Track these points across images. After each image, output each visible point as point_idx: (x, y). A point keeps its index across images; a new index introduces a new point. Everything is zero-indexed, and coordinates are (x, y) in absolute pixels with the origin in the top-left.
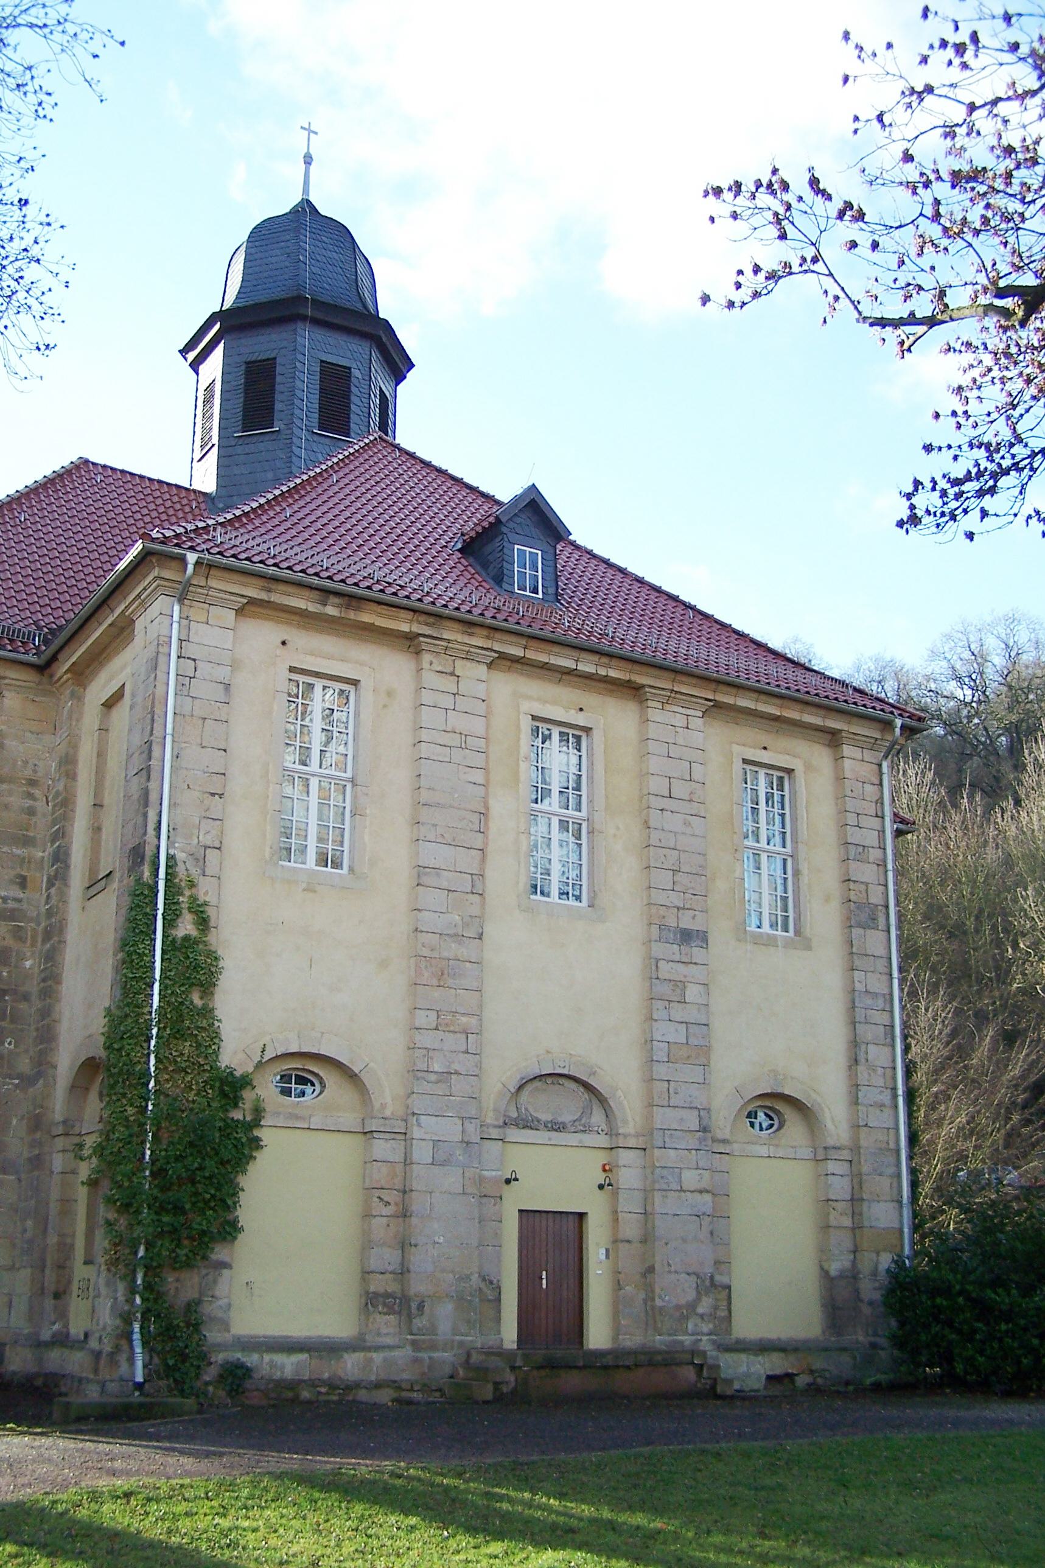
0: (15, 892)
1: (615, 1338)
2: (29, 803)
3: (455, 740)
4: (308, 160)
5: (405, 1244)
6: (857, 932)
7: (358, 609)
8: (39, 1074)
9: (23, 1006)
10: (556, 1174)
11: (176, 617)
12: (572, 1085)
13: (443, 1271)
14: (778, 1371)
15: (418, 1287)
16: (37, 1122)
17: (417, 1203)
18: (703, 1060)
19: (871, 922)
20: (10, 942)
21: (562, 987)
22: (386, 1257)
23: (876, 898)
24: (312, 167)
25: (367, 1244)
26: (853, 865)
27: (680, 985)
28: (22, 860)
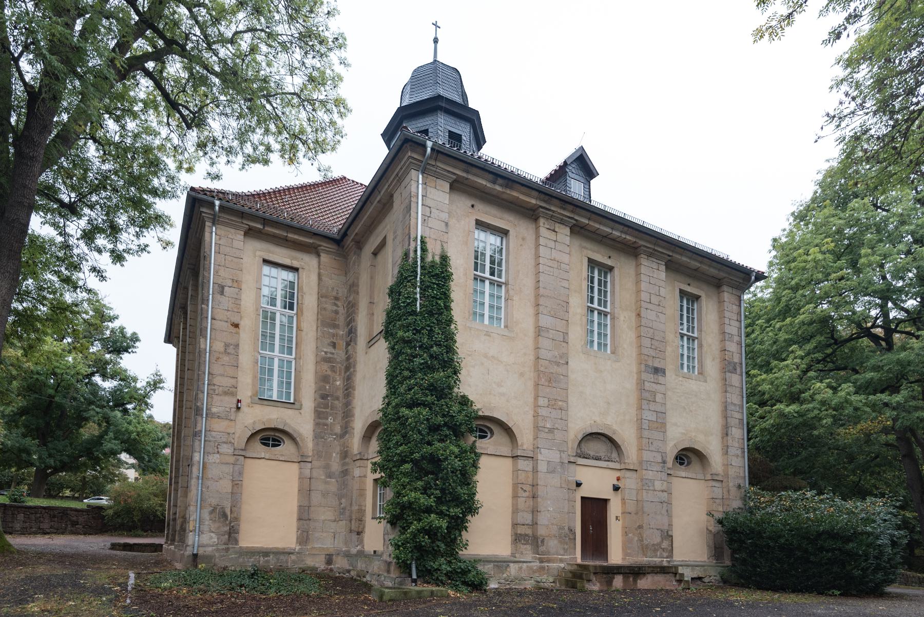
0: (330, 349)
1: (623, 559)
2: (335, 308)
3: (555, 265)
4: (436, 41)
5: (535, 511)
6: (728, 374)
7: (511, 188)
8: (346, 433)
9: (336, 402)
10: (596, 481)
11: (420, 182)
12: (604, 439)
13: (552, 524)
14: (695, 576)
15: (541, 531)
16: (345, 454)
17: (541, 491)
18: (663, 430)
19: (734, 371)
20: (329, 373)
21: (600, 391)
22: (527, 518)
23: (736, 360)
24: (439, 45)
25: (515, 511)
26: (727, 343)
27: (654, 394)
28: (333, 335)
